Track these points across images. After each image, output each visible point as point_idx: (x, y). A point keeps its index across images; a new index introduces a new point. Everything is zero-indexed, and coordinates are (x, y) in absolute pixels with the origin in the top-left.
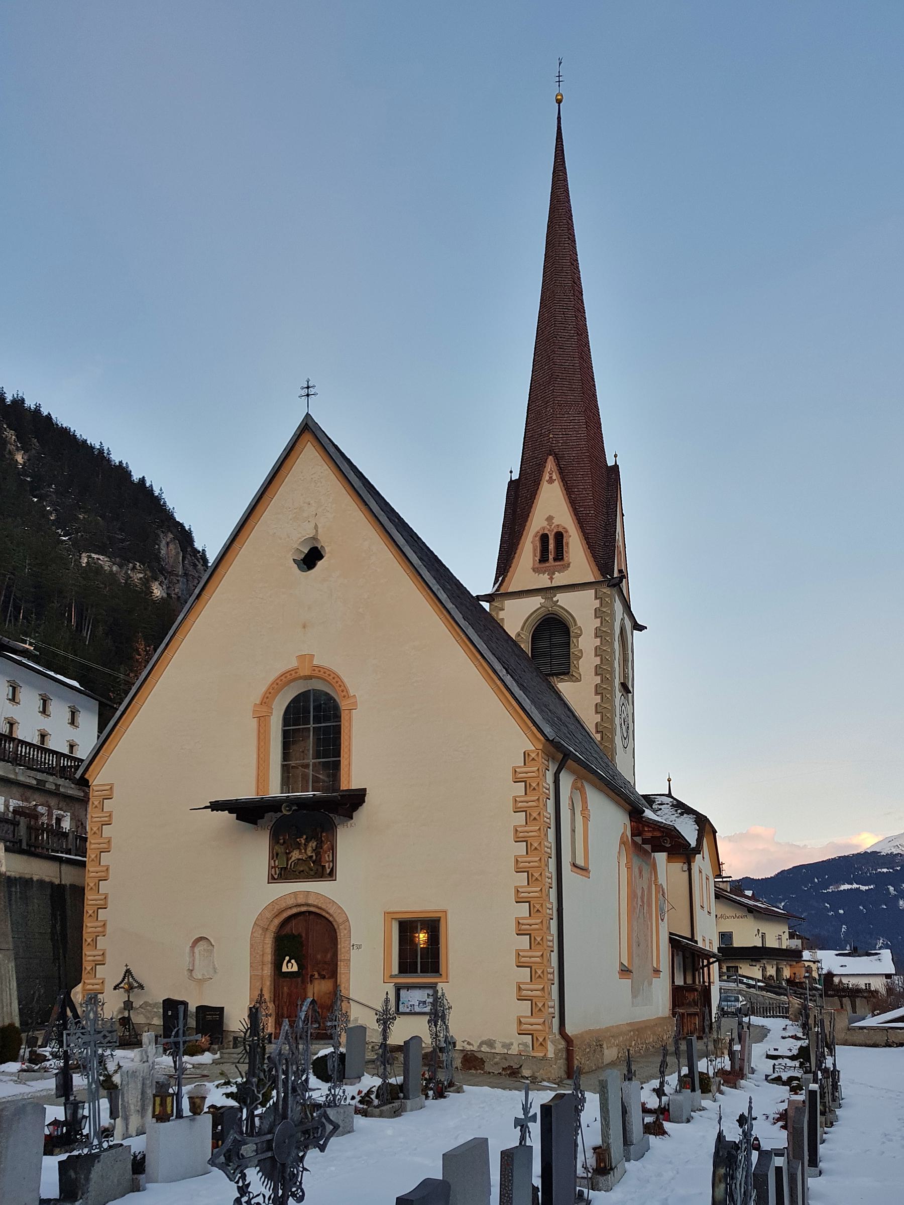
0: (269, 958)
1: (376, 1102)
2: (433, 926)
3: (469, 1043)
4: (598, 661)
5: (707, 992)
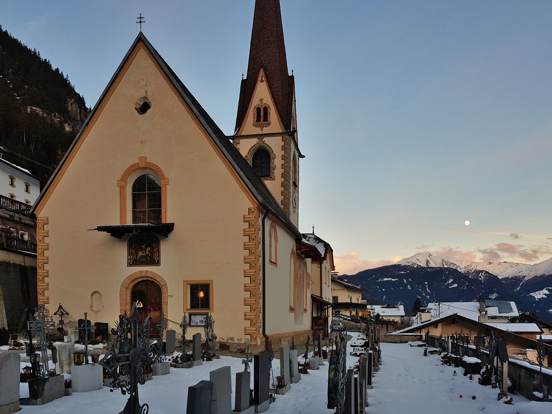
0: (129, 301)
1: (180, 362)
2: (206, 287)
3: (222, 339)
5: (326, 319)
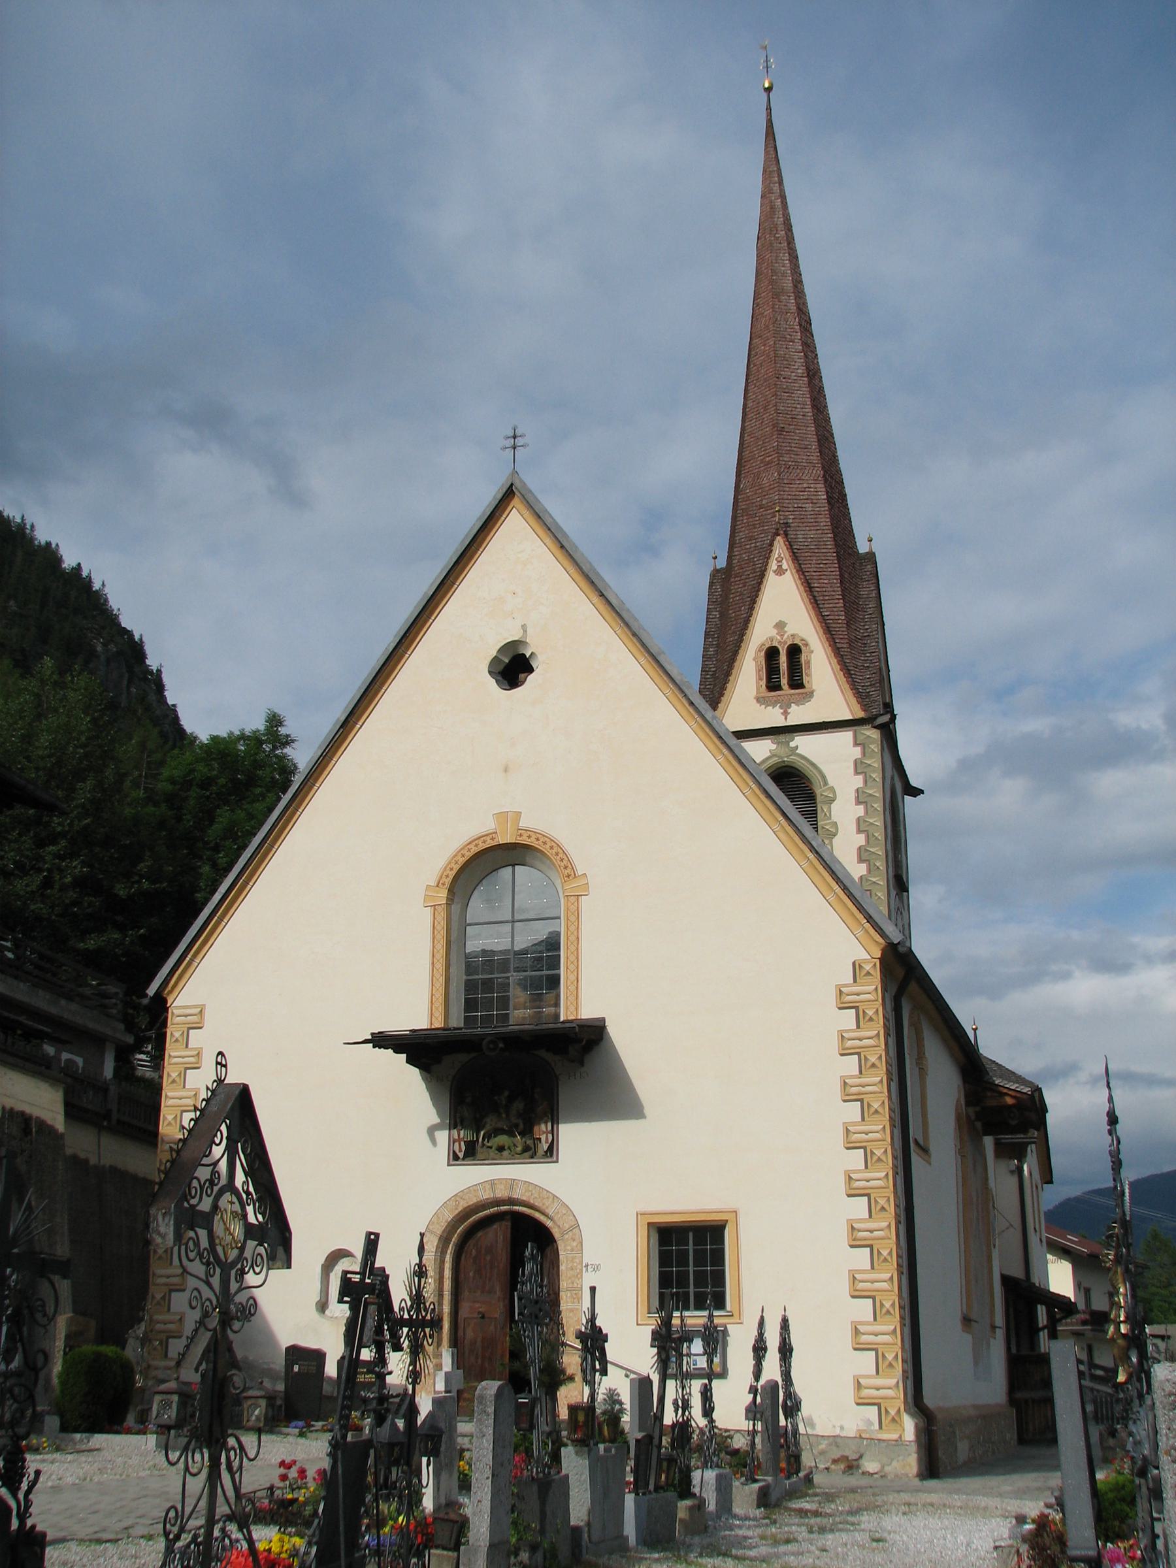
4: (861, 840)
